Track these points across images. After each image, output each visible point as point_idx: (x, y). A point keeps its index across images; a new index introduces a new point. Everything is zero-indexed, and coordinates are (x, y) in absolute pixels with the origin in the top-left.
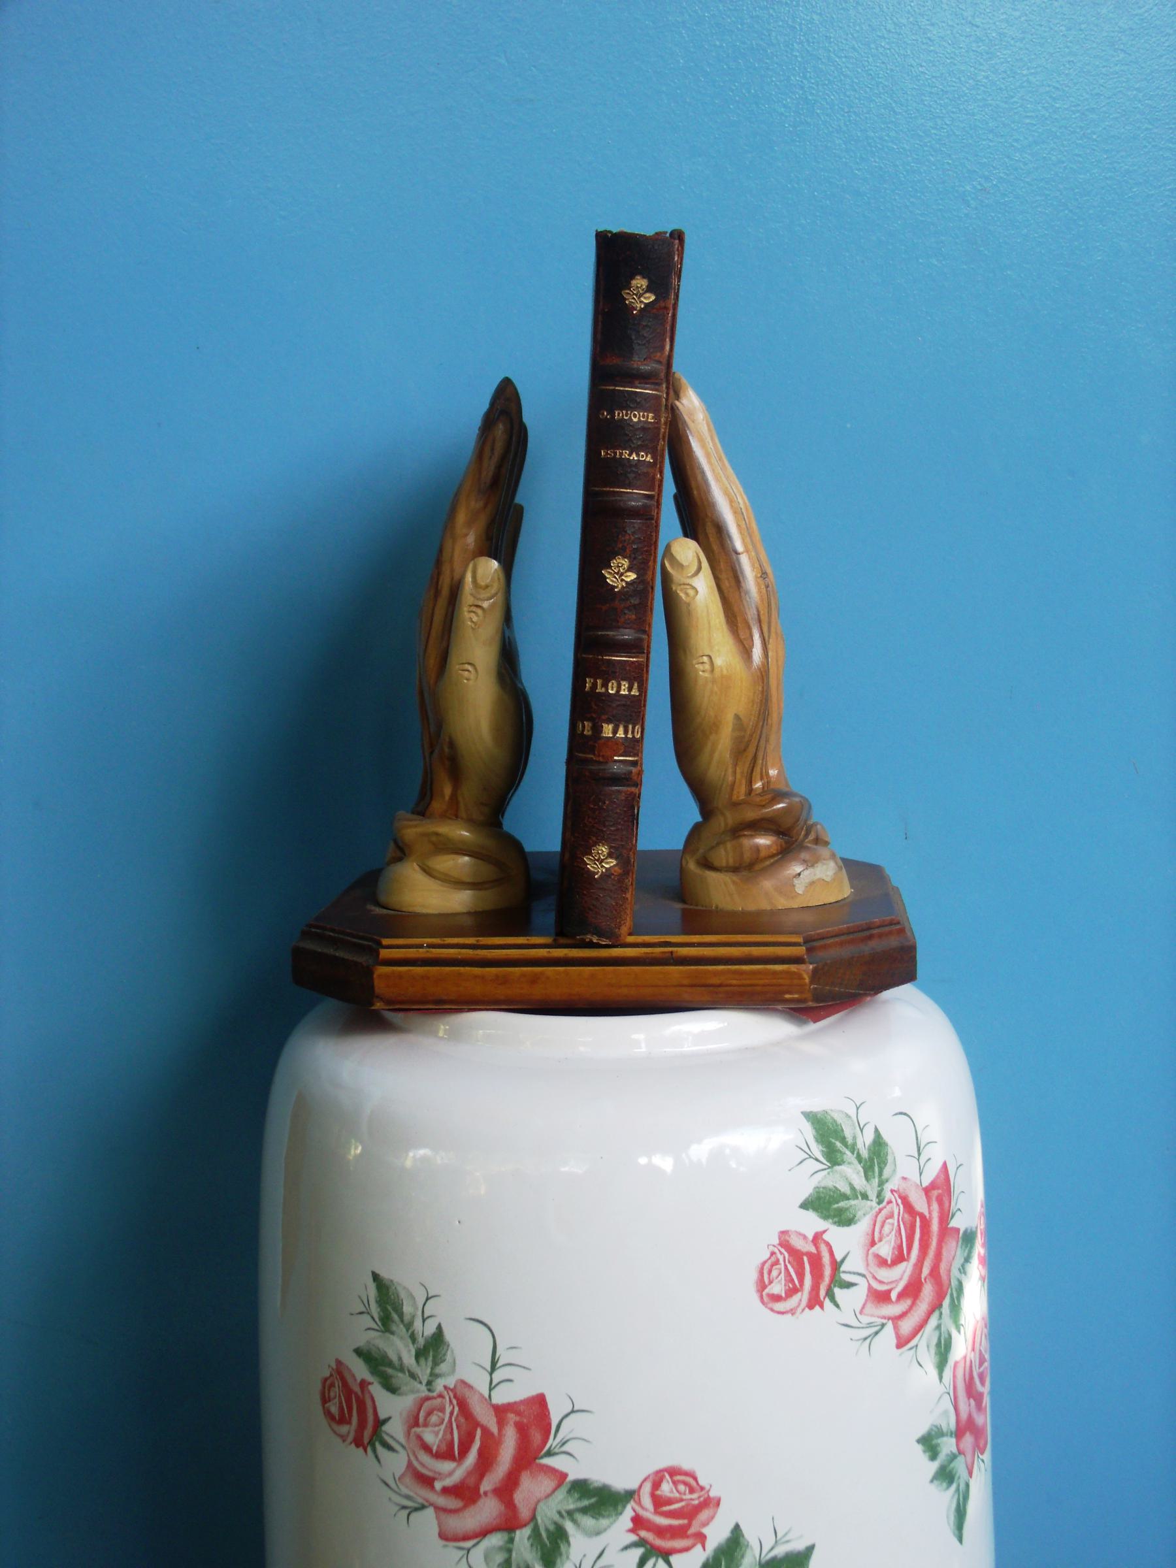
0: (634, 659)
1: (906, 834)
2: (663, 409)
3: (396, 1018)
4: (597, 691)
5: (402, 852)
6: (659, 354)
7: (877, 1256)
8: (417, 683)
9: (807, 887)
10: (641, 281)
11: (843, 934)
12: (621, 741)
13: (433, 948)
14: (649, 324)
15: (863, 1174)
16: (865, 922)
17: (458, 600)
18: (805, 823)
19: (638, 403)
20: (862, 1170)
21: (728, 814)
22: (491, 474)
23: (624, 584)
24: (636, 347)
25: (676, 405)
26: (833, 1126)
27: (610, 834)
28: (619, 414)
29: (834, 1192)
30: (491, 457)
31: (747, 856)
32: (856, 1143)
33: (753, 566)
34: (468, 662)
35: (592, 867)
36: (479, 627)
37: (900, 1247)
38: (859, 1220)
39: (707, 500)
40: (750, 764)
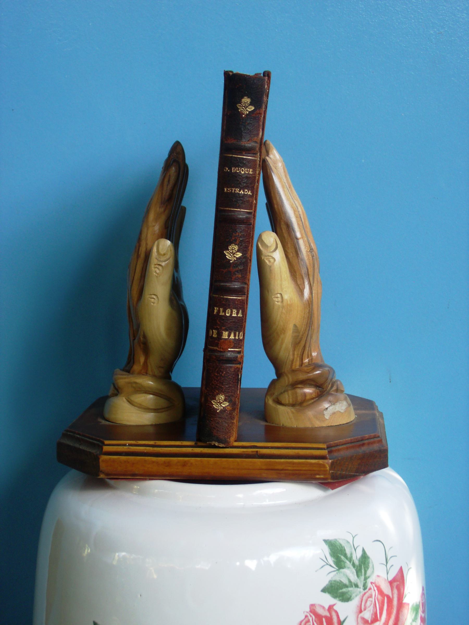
0: (240, 298)
1: (390, 379)
2: (258, 166)
3: (112, 482)
4: (220, 314)
5: (117, 391)
6: (256, 138)
7: (363, 619)
8: (127, 302)
9: (331, 415)
10: (247, 99)
11: (348, 443)
12: (232, 340)
13: (131, 446)
14: (251, 122)
15: (355, 573)
16: (360, 437)
17: (149, 262)
18: (331, 380)
19: (244, 164)
20: (355, 572)
21: (290, 376)
22: (168, 194)
23: (235, 259)
24: (244, 134)
25: (266, 159)
26: (340, 548)
27: (225, 389)
28: (234, 169)
29: (340, 583)
30: (168, 185)
31: (300, 399)
32: (352, 557)
33: (305, 245)
34: (153, 294)
35: (216, 406)
36: (159, 276)
37: (376, 614)
38: (353, 599)
39: (282, 210)
40: (302, 350)
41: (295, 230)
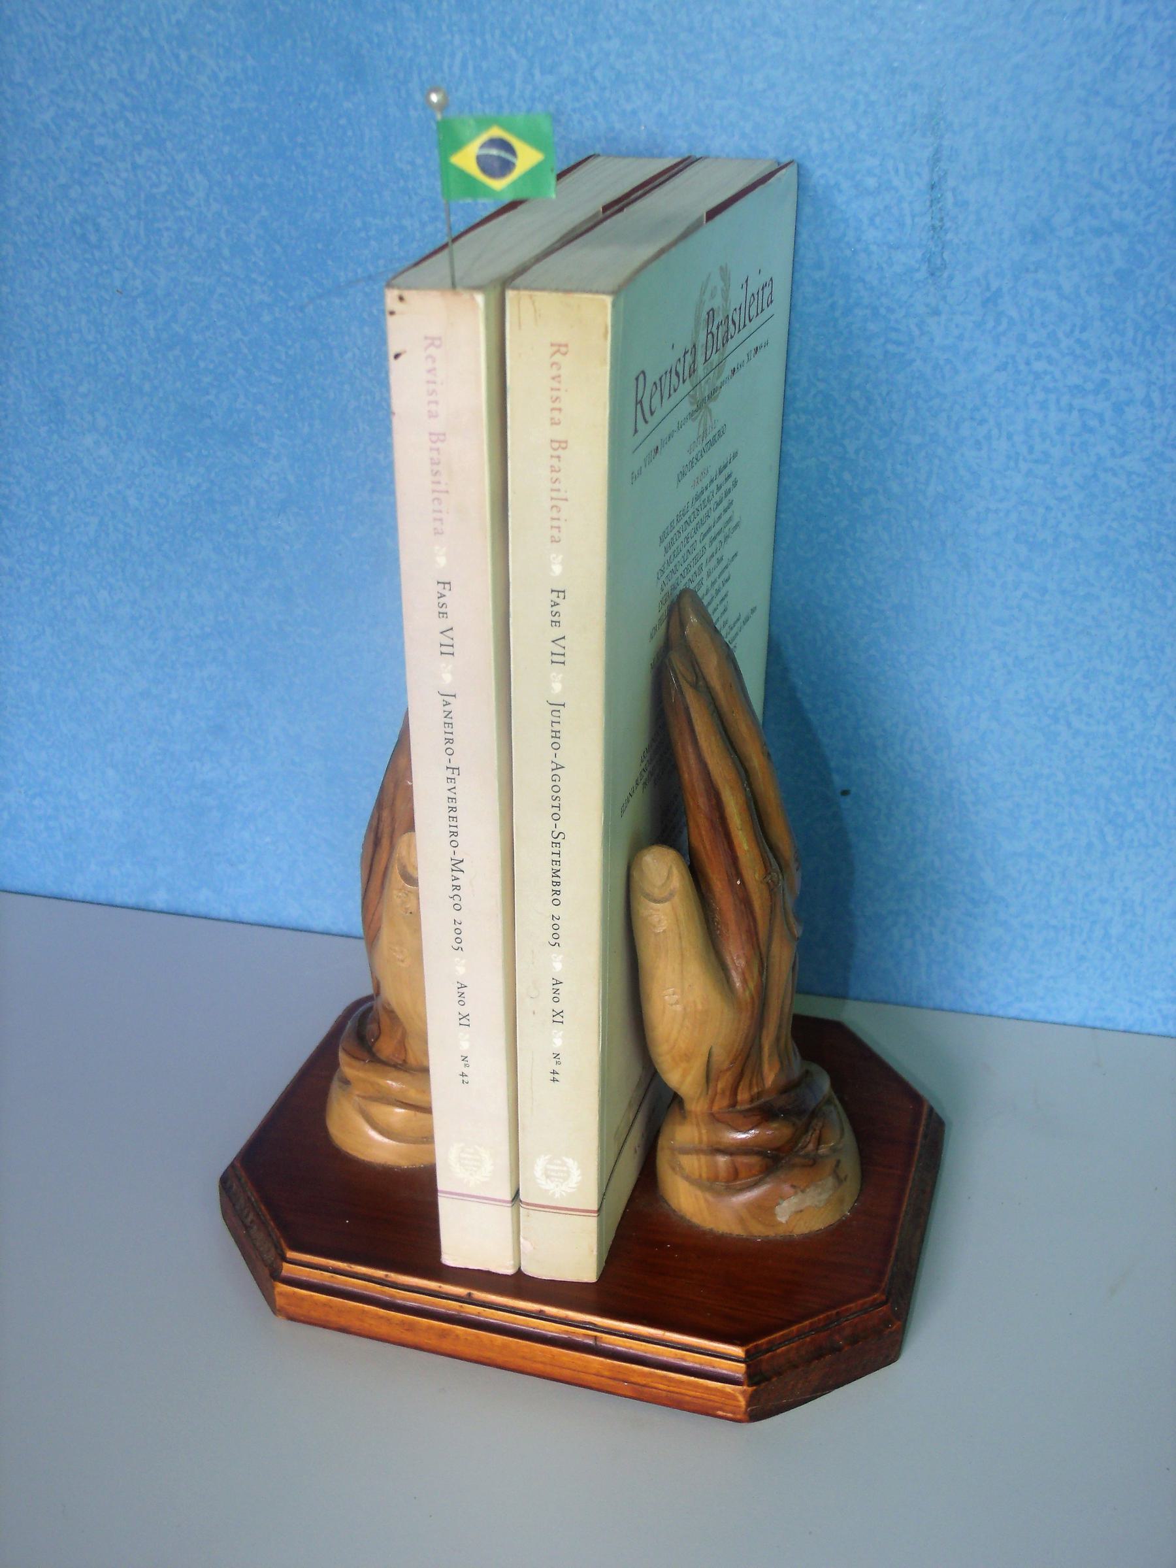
41: (509, 1113)
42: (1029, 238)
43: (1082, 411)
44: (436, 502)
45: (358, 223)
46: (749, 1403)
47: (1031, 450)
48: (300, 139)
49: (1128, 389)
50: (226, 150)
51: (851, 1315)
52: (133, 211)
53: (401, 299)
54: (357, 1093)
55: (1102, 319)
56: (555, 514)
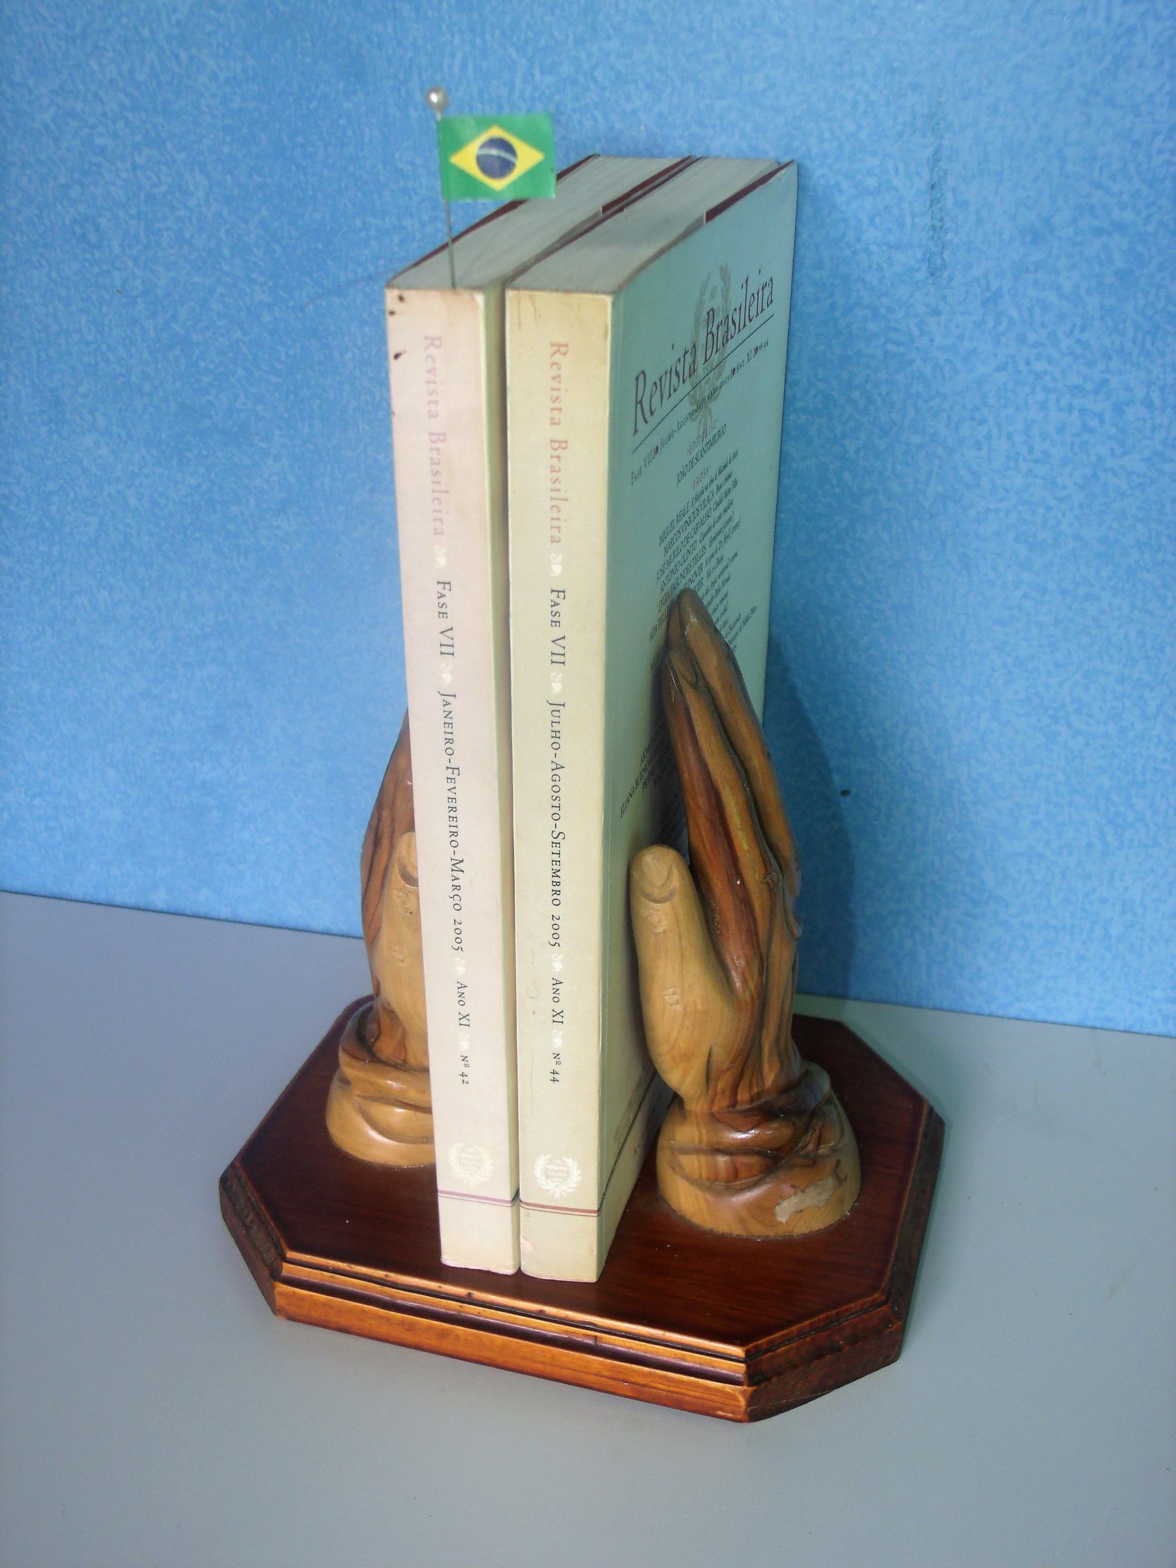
42: (1029, 238)
43: (1082, 411)
44: (436, 502)
45: (358, 223)
46: (749, 1403)
47: (1031, 450)
48: (300, 139)
49: (1128, 389)
50: (226, 150)
51: (851, 1315)
52: (133, 211)
53: (401, 299)
54: (357, 1093)
55: (1102, 319)
56: (555, 514)
